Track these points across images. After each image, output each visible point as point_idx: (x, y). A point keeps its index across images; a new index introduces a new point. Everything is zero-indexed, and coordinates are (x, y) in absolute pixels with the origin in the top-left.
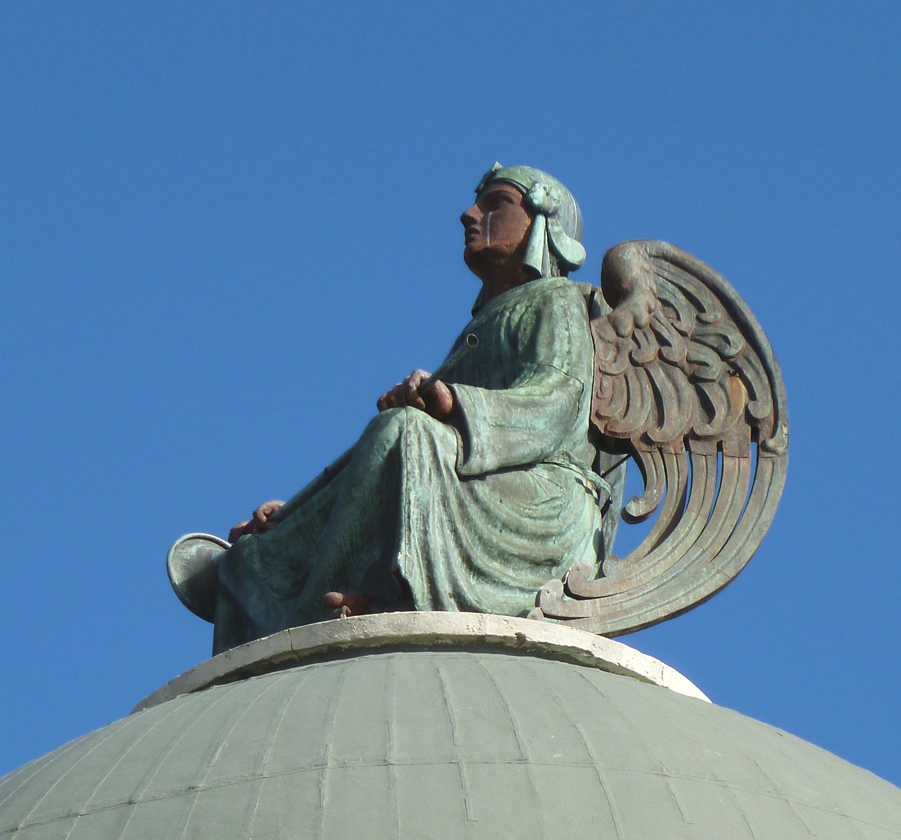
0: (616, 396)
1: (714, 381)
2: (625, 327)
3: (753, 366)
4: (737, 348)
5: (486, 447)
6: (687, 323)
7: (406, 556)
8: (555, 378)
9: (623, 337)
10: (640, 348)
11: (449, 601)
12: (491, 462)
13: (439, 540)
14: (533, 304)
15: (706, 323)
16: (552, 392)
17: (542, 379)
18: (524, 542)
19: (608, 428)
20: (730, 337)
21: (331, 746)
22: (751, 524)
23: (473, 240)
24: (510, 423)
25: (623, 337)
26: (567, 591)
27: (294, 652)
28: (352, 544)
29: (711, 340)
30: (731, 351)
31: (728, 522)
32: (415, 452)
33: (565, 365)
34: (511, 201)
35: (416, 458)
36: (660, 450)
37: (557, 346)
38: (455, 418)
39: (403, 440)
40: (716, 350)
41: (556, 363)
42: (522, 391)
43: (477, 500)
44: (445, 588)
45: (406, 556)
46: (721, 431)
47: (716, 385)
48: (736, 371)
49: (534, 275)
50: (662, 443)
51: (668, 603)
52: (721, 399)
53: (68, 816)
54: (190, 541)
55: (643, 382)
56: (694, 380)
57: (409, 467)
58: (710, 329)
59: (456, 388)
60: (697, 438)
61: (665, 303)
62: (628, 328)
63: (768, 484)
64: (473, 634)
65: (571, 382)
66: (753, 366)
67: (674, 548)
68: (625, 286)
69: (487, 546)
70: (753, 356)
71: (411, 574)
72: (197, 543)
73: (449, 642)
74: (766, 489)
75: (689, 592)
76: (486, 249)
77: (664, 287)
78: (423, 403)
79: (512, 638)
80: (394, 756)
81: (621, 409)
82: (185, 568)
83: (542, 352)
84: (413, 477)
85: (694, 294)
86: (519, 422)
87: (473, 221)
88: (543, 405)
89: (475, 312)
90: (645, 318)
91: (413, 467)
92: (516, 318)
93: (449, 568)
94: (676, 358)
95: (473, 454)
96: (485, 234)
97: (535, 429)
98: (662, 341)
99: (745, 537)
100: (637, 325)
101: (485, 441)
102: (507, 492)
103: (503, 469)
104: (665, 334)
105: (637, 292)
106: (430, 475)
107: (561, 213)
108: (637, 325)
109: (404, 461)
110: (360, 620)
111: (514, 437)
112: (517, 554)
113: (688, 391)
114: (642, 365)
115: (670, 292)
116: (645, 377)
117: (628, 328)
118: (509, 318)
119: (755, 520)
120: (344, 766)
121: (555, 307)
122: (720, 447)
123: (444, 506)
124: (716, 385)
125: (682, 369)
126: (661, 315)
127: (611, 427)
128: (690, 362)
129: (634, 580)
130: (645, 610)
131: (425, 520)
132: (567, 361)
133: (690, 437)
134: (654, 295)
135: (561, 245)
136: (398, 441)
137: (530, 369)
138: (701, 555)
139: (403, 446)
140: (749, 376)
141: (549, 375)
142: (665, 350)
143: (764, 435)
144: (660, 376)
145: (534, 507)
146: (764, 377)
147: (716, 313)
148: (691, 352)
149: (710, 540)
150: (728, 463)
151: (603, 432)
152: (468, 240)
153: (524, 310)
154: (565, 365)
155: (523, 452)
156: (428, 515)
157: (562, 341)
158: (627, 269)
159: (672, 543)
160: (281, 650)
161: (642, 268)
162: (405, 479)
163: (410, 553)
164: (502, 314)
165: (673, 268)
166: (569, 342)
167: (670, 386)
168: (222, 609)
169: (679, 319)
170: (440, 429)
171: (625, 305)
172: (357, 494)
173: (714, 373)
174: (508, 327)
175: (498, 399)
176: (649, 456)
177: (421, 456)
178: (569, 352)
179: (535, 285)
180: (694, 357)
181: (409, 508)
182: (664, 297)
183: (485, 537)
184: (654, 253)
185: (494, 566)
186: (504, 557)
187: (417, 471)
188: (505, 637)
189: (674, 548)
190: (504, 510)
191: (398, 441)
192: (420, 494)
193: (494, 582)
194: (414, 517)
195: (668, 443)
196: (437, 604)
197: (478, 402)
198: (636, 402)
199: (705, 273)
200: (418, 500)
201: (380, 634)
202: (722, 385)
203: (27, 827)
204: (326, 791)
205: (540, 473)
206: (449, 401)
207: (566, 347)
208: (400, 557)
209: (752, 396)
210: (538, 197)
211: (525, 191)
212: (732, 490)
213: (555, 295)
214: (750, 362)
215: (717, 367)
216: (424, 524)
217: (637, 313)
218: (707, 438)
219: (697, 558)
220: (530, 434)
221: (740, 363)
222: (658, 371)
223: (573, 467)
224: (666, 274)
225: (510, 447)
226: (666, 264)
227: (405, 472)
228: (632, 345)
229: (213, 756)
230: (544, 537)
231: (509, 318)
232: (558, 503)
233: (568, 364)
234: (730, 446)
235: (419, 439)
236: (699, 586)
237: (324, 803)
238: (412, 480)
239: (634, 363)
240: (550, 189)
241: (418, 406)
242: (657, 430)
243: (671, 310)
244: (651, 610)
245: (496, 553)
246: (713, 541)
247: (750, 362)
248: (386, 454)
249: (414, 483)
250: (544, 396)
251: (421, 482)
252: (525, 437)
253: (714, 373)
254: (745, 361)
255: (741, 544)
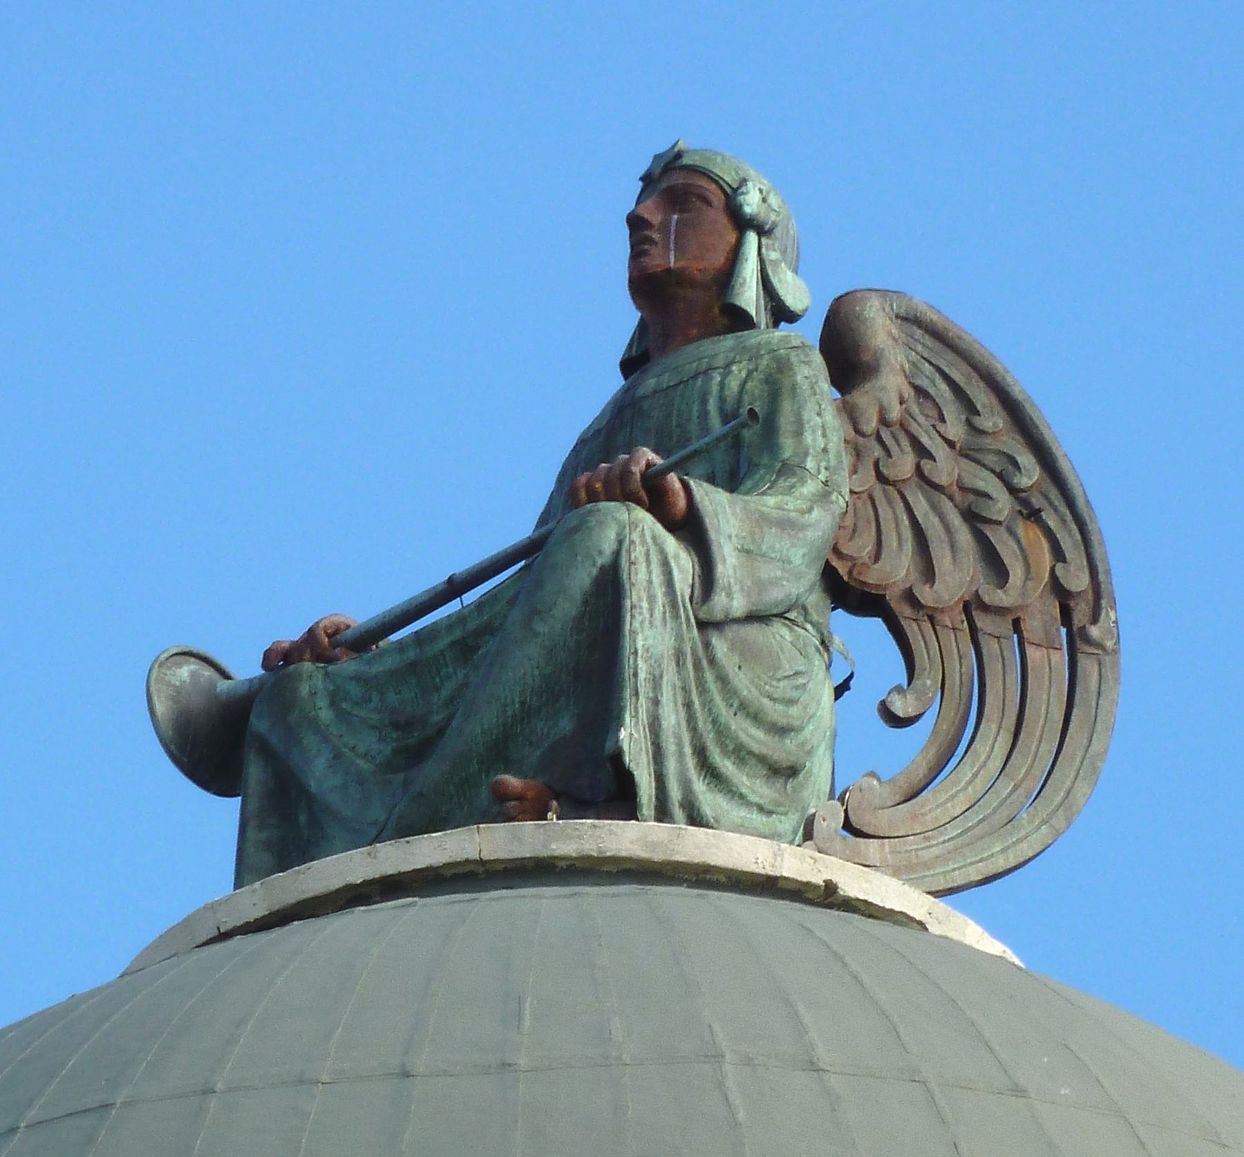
0: (860, 524)
1: (999, 523)
2: (868, 422)
3: (1056, 510)
4: (1030, 478)
5: (732, 580)
6: (955, 429)
7: (631, 734)
8: (810, 487)
9: (863, 435)
10: (890, 456)
11: (678, 813)
12: (739, 606)
13: (671, 718)
14: (761, 367)
15: (983, 433)
16: (810, 510)
17: (792, 487)
18: (760, 734)
19: (855, 573)
20: (1019, 459)
21: (716, 1027)
22: (1080, 754)
23: (644, 253)
24: (760, 549)
25: (863, 435)
26: (848, 826)
27: (481, 862)
28: (522, 703)
29: (990, 459)
30: (1024, 481)
31: (1044, 747)
32: (641, 575)
33: (823, 470)
34: (708, 203)
35: (642, 584)
36: (932, 619)
37: (808, 438)
38: (690, 528)
39: (624, 553)
40: (1000, 476)
41: (810, 464)
42: (771, 501)
43: (712, 661)
44: (675, 793)
45: (631, 734)
46: (1020, 601)
47: (1002, 529)
48: (1033, 515)
49: (740, 320)
50: (935, 609)
51: (981, 860)
52: (1014, 553)
53: (301, 1082)
54: (177, 658)
55: (898, 512)
56: (973, 518)
57: (634, 597)
58: (987, 442)
59: (692, 483)
60: (986, 608)
61: (920, 392)
62: (871, 424)
63: (1096, 694)
64: (763, 872)
65: (834, 497)
66: (1056, 510)
67: (976, 775)
68: (866, 357)
69: (722, 733)
70: (1054, 494)
71: (638, 764)
72: (188, 663)
73: (723, 879)
74: (1094, 704)
75: (1008, 847)
76: (669, 270)
77: (919, 369)
78: (645, 498)
79: (817, 887)
80: (824, 1056)
81: (870, 548)
82: (174, 699)
83: (788, 447)
84: (641, 613)
85: (962, 385)
86: (772, 548)
87: (649, 225)
88: (804, 527)
89: (631, 365)
90: (895, 413)
91: (640, 600)
92: (733, 384)
93: (680, 763)
94: (943, 480)
95: (717, 589)
96: (666, 247)
97: (790, 562)
98: (922, 452)
99: (1073, 774)
100: (884, 422)
101: (731, 572)
102: (749, 655)
103: (755, 617)
104: (925, 440)
105: (885, 371)
106: (664, 613)
107: (778, 232)
108: (884, 422)
109: (627, 586)
110: (595, 826)
111: (768, 571)
112: (757, 752)
113: (964, 536)
114: (894, 484)
115: (927, 377)
116: (900, 505)
117: (871, 424)
118: (722, 385)
119: (1083, 750)
120: (748, 1061)
121: (799, 378)
122: (1016, 624)
123: (678, 664)
124: (1002, 529)
125: (951, 498)
126: (915, 410)
127: (860, 573)
128: (963, 488)
129: (929, 817)
130: (952, 867)
131: (656, 682)
132: (823, 464)
133: (972, 606)
134: (906, 377)
135: (780, 281)
136: (617, 554)
137: (769, 468)
138: (1012, 792)
139: (624, 563)
140: (1051, 523)
141: (803, 481)
142: (927, 465)
143: (1081, 614)
144: (921, 506)
145: (775, 683)
146: (1074, 527)
147: (993, 420)
148: (963, 474)
149: (1023, 771)
150: (1031, 652)
151: (846, 578)
152: (637, 254)
153: (744, 374)
154: (823, 470)
155: (775, 596)
156: (661, 677)
157: (814, 432)
158: (869, 332)
159: (972, 767)
160: (460, 856)
161: (890, 333)
162: (629, 615)
163: (638, 732)
164: (707, 372)
165: (928, 340)
166: (824, 435)
167: (936, 520)
168: (255, 772)
169: (943, 420)
170: (671, 543)
171: (868, 386)
172: (541, 627)
173: (1000, 511)
174: (722, 400)
175: (745, 508)
176: (914, 625)
177: (650, 582)
178: (825, 450)
179: (750, 338)
180: (969, 482)
181: (636, 660)
182: (918, 382)
183: (722, 720)
184: (902, 312)
185: (727, 766)
186: (741, 754)
187: (645, 605)
188: (808, 884)
189: (976, 775)
190: (742, 681)
191: (617, 554)
192: (650, 641)
193: (730, 791)
194: (642, 675)
195: (942, 611)
196: (663, 814)
197: (721, 509)
198: (890, 540)
199: (977, 355)
200: (647, 650)
201: (624, 854)
202: (1012, 532)
203: (229, 1090)
204: (736, 1098)
205: (780, 631)
206: (681, 503)
207: (821, 443)
208: (623, 734)
209: (1059, 555)
210: (751, 203)
211: (729, 190)
212: (1045, 697)
213: (794, 359)
214: (1051, 504)
215: (1002, 505)
216: (654, 689)
217: (885, 403)
218: (1000, 611)
219: (1009, 795)
220: (783, 570)
221: (1037, 501)
222: (917, 497)
223: (809, 627)
224: (919, 348)
225: (761, 586)
226: (919, 333)
227: (628, 604)
228: (878, 452)
229: (520, 1018)
230: (782, 731)
231: (722, 385)
232: (801, 681)
233: (826, 469)
234: (1033, 626)
235: (647, 554)
236: (1019, 841)
237: (741, 1115)
238: (639, 618)
239: (882, 478)
240: (768, 193)
241: (639, 502)
242: (927, 587)
243: (929, 404)
244: (959, 868)
245: (731, 748)
246: (1028, 772)
247: (1051, 504)
248: (595, 571)
249: (642, 622)
250: (803, 512)
251: (651, 623)
252: (779, 573)
253: (1000, 511)
254: (1042, 500)
255: (1069, 783)
